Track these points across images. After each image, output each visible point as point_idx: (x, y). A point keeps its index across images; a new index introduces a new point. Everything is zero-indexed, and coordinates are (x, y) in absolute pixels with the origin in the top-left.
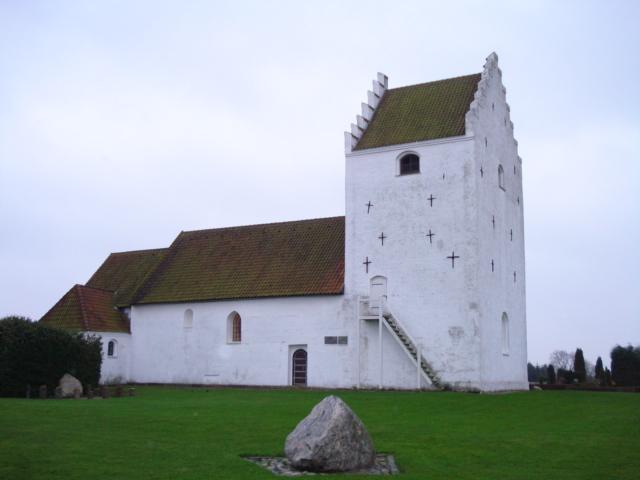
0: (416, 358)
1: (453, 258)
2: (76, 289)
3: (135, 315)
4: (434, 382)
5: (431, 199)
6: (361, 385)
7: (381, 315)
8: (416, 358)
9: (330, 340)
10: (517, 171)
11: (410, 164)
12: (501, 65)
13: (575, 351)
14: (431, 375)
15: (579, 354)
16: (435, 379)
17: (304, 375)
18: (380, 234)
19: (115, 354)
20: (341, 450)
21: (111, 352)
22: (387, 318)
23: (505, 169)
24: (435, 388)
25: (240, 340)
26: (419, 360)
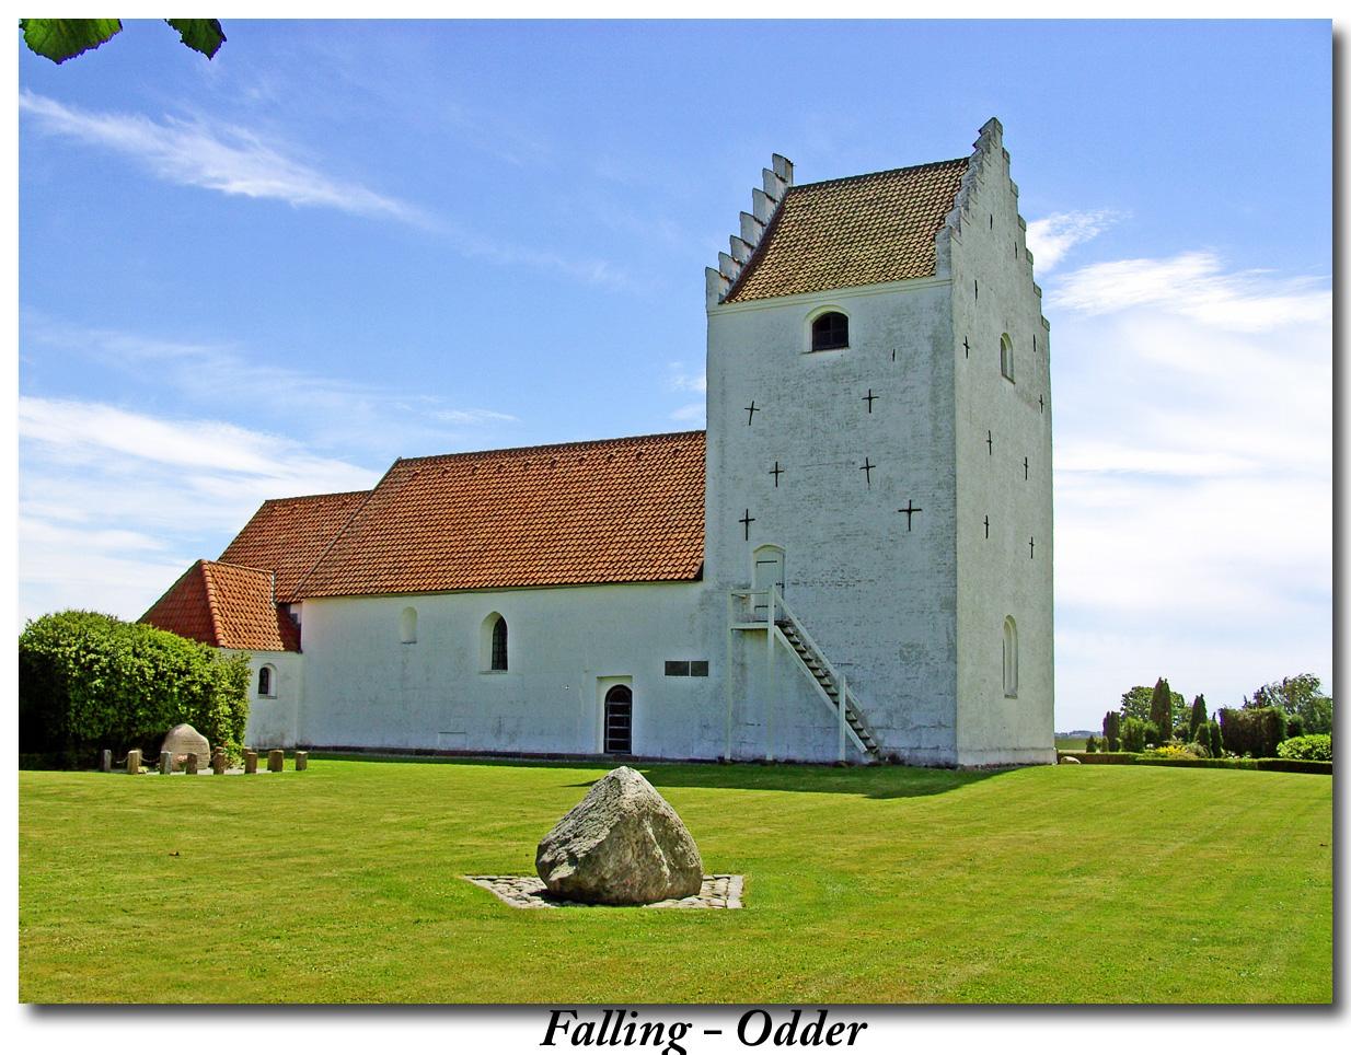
0: (837, 704)
1: (910, 511)
2: (1105, 720)
3: (1097, 727)
4: (870, 748)
5: (870, 398)
6: (932, 759)
7: (771, 621)
8: (837, 704)
9: (674, 668)
10: (1041, 347)
11: (830, 331)
12: (1008, 140)
13: (1152, 684)
14: (865, 733)
15: (1200, 701)
16: (872, 742)
17: (627, 734)
18: (770, 466)
19: (273, 690)
20: (634, 865)
21: (264, 687)
22: (782, 624)
23: (1015, 342)
24: (871, 759)
25: (505, 668)
26: (843, 707)
